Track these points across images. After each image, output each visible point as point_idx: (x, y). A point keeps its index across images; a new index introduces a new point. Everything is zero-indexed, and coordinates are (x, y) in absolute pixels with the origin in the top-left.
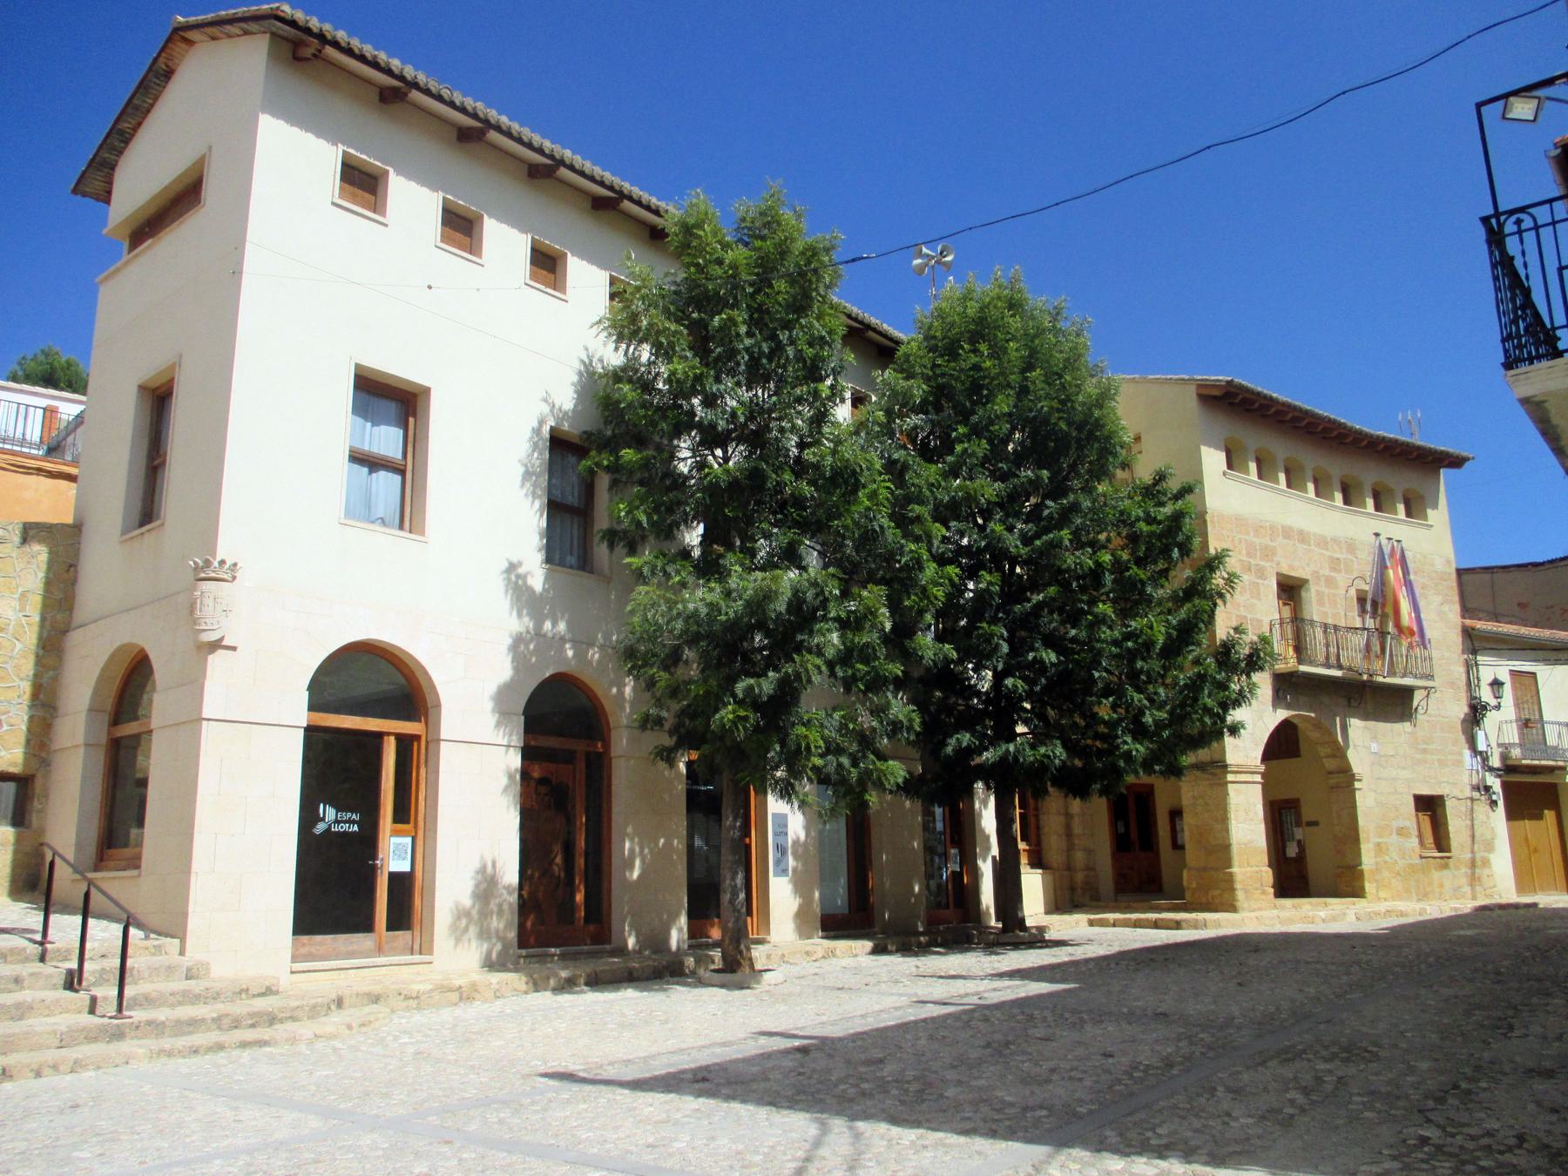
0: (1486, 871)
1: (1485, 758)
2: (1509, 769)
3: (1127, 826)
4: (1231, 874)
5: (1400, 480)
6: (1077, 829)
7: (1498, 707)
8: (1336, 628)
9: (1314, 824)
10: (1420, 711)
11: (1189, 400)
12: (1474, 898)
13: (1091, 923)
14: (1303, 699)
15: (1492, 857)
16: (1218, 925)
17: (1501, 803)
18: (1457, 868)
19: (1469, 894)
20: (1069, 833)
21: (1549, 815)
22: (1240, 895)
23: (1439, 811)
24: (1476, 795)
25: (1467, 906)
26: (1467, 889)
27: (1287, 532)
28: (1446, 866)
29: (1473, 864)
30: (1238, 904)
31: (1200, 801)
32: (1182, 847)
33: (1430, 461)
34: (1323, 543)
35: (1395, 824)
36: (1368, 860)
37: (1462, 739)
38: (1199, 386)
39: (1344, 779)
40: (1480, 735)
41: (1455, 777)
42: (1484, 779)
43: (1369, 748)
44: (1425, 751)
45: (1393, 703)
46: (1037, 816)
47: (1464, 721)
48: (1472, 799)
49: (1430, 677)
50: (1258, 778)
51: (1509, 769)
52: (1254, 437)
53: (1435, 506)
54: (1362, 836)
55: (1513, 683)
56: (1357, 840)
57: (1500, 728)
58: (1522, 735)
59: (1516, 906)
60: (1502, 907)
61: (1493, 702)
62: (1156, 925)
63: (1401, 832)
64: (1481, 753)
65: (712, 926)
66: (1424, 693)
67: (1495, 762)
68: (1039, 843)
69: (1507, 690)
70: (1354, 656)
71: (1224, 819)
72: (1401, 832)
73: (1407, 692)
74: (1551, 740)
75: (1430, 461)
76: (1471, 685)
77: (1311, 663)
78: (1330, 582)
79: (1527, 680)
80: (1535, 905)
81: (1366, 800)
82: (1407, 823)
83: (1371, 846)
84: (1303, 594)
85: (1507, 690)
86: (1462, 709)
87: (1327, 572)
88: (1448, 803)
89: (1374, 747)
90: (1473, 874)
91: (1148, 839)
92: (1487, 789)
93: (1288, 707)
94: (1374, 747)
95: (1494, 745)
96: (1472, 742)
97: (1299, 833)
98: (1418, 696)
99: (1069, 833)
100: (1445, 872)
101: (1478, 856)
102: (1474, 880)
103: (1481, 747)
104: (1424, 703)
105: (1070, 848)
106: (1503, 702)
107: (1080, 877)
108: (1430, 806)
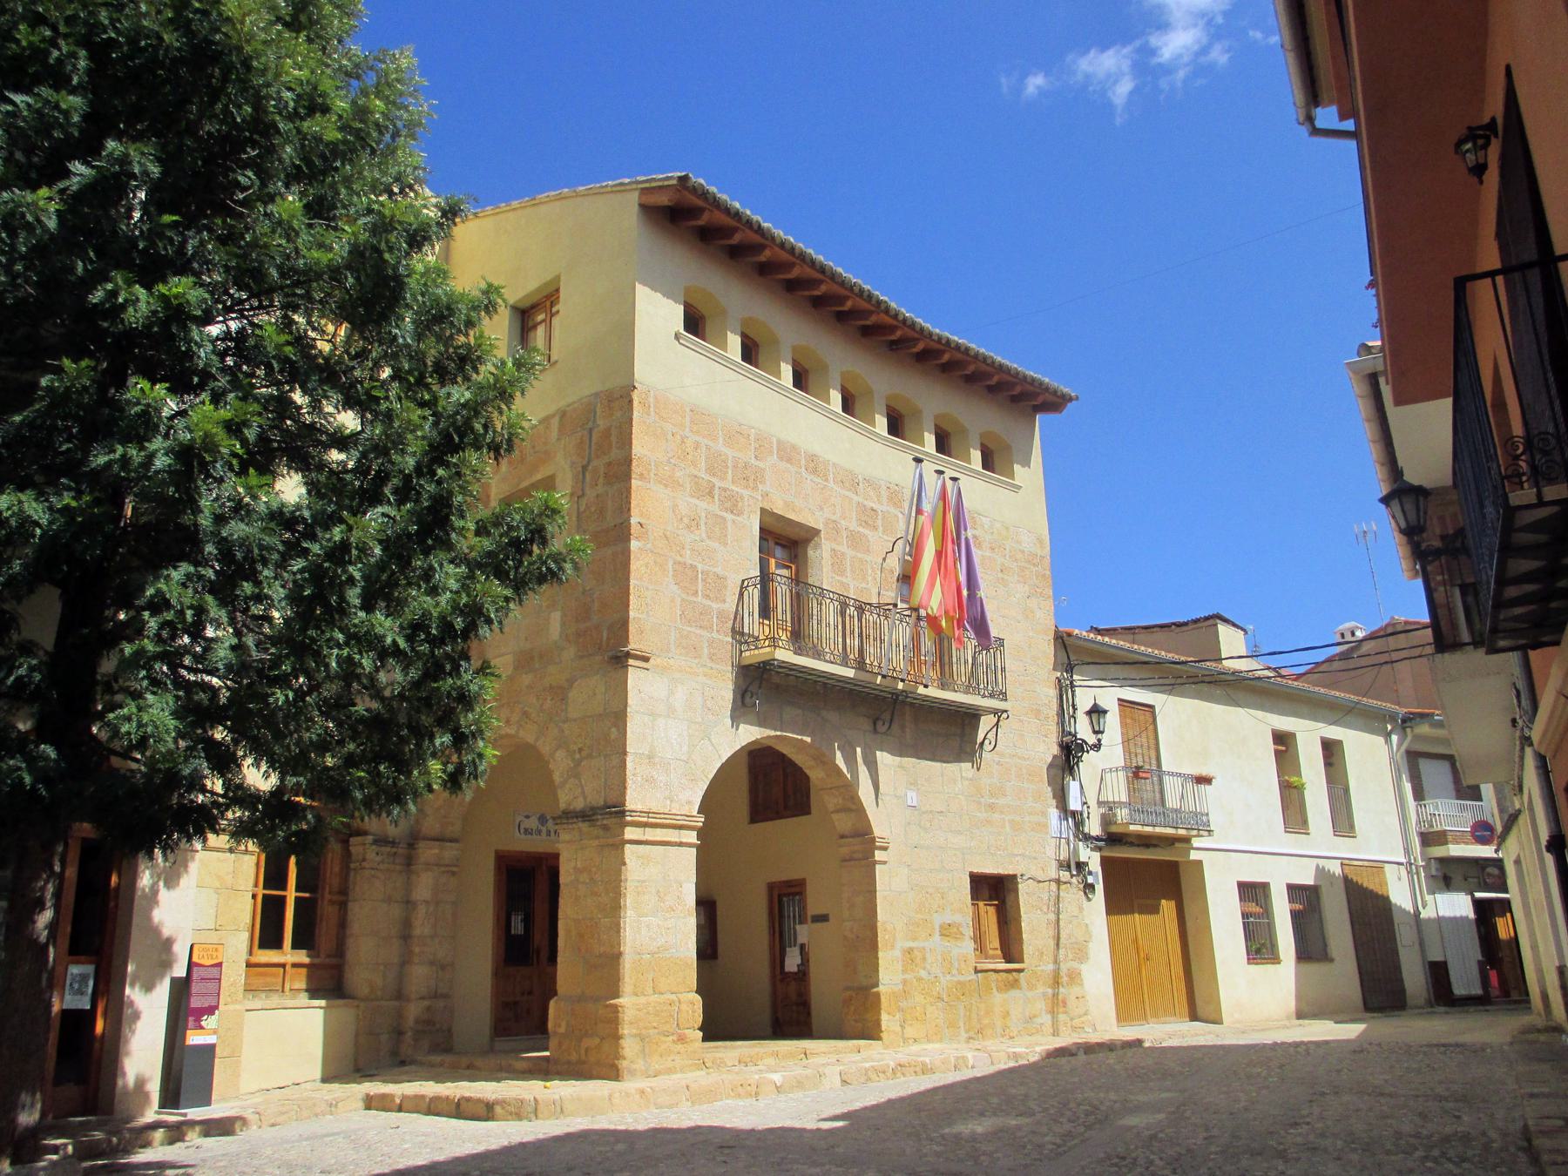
0: (1075, 990)
1: (1077, 819)
2: (1113, 838)
3: (528, 921)
4: (615, 1009)
5: (977, 417)
6: (421, 928)
8: (861, 608)
9: (823, 918)
10: (987, 747)
11: (627, 212)
12: (1055, 1033)
13: (370, 1103)
14: (790, 712)
15: (1084, 967)
16: (559, 1109)
17: (1100, 888)
18: (1031, 987)
19: (1048, 1028)
21: (1167, 906)
22: (629, 1046)
23: (1010, 900)
24: (1065, 875)
25: (1031, 1048)
26: (1046, 1019)
27: (787, 453)
28: (1015, 984)
29: (1056, 982)
30: (623, 1064)
31: (584, 877)
33: (1025, 398)
34: (852, 482)
35: (938, 920)
36: (890, 976)
37: (1048, 791)
39: (860, 846)
40: (1073, 787)
41: (1033, 847)
42: (1076, 851)
44: (992, 807)
45: (950, 731)
46: (343, 906)
47: (1050, 766)
48: (1058, 882)
49: (1003, 696)
50: (692, 837)
51: (1113, 838)
52: (738, 299)
53: (1026, 463)
54: (882, 937)
55: (1123, 717)
56: (873, 946)
57: (1101, 778)
58: (1131, 791)
59: (1109, 1047)
60: (1089, 1048)
61: (1091, 739)
62: (460, 1110)
63: (947, 931)
64: (1074, 813)
66: (992, 719)
67: (1094, 828)
68: (340, 951)
69: (1112, 722)
70: (893, 654)
71: (614, 908)
72: (947, 931)
73: (966, 719)
74: (1172, 801)
75: (1025, 398)
76: (1064, 713)
77: (818, 655)
78: (856, 540)
79: (1142, 716)
80: (1139, 1042)
81: (893, 881)
82: (957, 918)
83: (897, 953)
84: (810, 552)
85: (1112, 722)
86: (1049, 749)
87: (853, 526)
88: (1023, 888)
89: (912, 797)
90: (1055, 995)
92: (1081, 866)
93: (762, 723)
94: (912, 797)
95: (1092, 803)
96: (1061, 797)
97: (803, 933)
98: (986, 722)
100: (1014, 993)
101: (1064, 967)
102: (1056, 1004)
103: (1074, 804)
104: (991, 736)
106: (1105, 739)
107: (413, 1011)
108: (994, 890)
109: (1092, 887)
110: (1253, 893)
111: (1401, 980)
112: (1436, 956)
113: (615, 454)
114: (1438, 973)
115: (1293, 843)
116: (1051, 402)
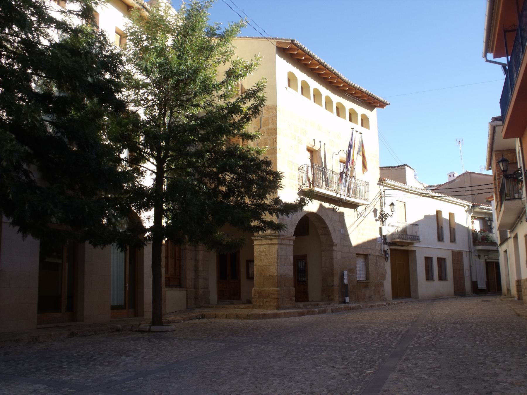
6: (201, 268)
7: (392, 216)
17: (389, 258)
20: (196, 271)
31: (263, 254)
32: (252, 278)
38: (277, 42)
43: (340, 231)
49: (368, 200)
50: (292, 243)
61: (391, 213)
65: (226, 190)
91: (235, 275)
99: (196, 271)
105: (197, 277)
109: (387, 258)
110: (428, 260)
111: (465, 286)
112: (474, 279)
113: (270, 126)
114: (474, 284)
115: (439, 245)
116: (382, 104)
